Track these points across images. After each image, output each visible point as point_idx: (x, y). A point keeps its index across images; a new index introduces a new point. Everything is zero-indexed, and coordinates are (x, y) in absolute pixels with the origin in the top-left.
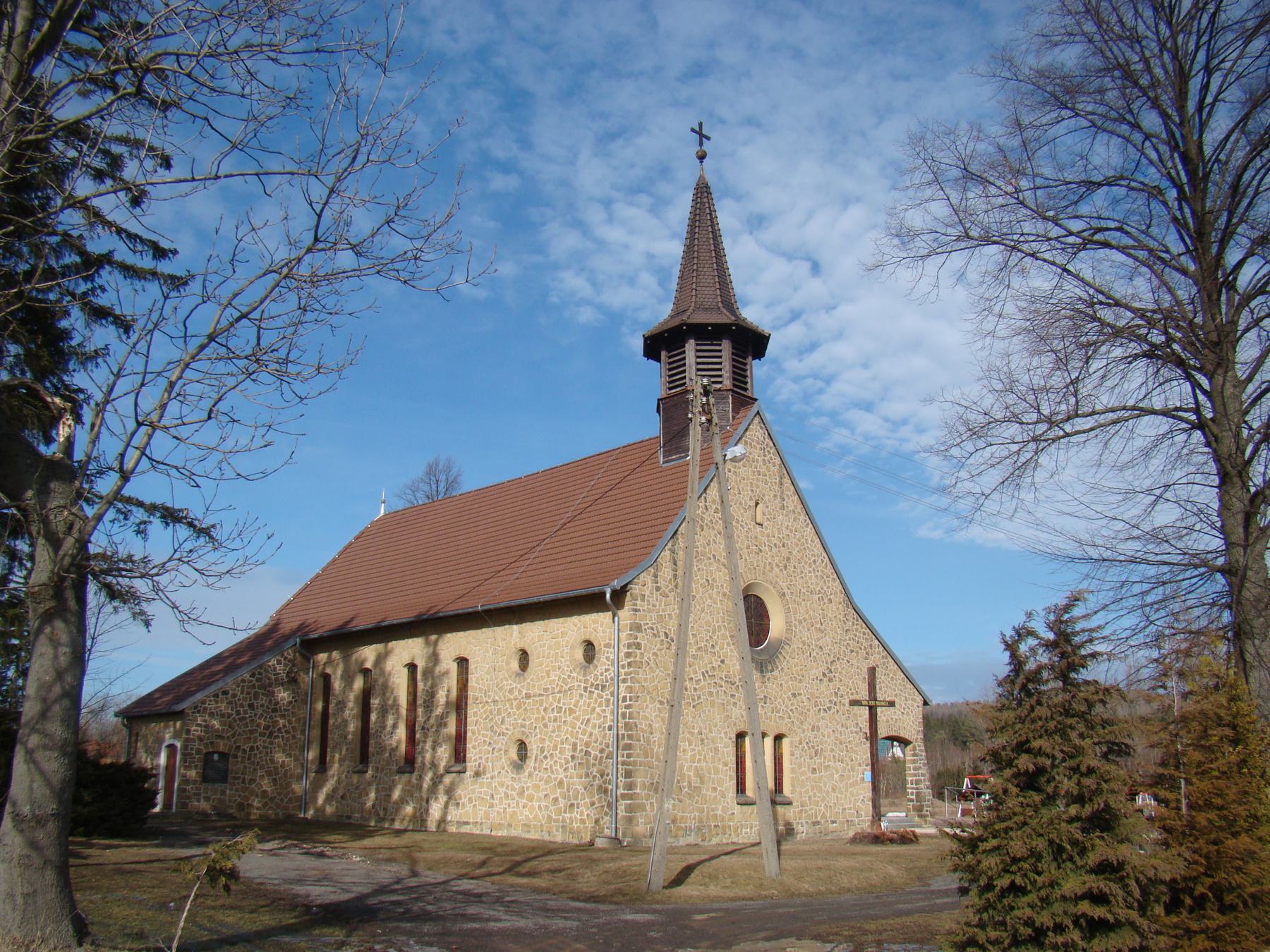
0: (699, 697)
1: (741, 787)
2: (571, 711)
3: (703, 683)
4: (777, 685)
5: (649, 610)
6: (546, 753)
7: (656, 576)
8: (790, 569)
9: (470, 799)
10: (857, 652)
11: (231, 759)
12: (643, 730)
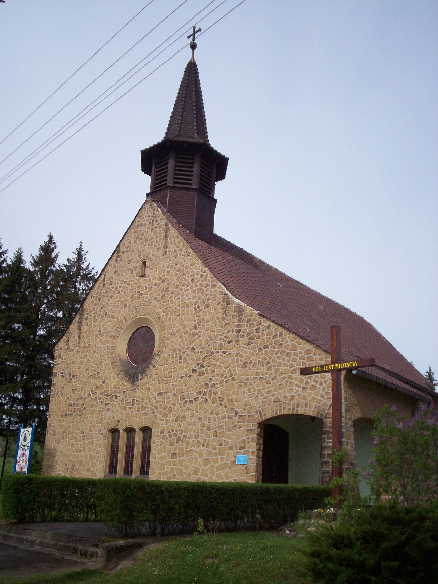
7: (68, 341)
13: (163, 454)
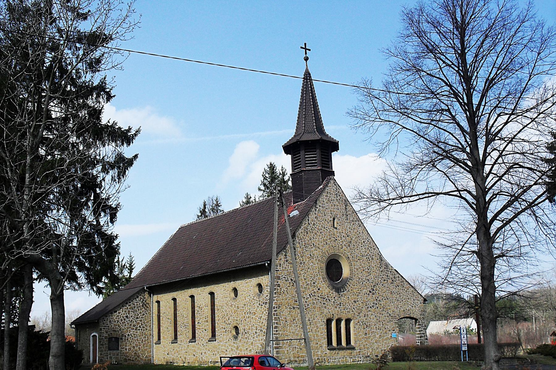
0: (308, 305)
1: (330, 342)
2: (255, 314)
3: (310, 299)
4: (347, 297)
5: (283, 270)
6: (246, 331)
7: (286, 255)
8: (352, 246)
9: (218, 352)
10: (387, 281)
11: (120, 340)
12: (282, 320)
13: (360, 333)
